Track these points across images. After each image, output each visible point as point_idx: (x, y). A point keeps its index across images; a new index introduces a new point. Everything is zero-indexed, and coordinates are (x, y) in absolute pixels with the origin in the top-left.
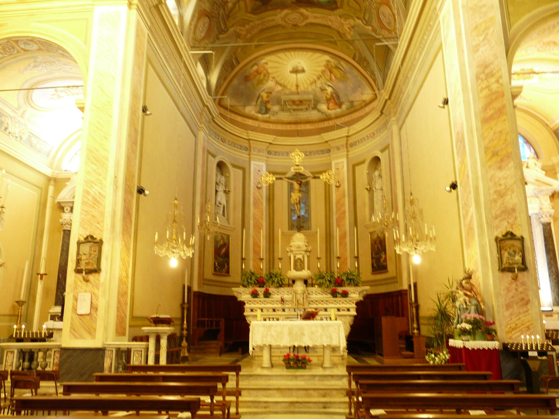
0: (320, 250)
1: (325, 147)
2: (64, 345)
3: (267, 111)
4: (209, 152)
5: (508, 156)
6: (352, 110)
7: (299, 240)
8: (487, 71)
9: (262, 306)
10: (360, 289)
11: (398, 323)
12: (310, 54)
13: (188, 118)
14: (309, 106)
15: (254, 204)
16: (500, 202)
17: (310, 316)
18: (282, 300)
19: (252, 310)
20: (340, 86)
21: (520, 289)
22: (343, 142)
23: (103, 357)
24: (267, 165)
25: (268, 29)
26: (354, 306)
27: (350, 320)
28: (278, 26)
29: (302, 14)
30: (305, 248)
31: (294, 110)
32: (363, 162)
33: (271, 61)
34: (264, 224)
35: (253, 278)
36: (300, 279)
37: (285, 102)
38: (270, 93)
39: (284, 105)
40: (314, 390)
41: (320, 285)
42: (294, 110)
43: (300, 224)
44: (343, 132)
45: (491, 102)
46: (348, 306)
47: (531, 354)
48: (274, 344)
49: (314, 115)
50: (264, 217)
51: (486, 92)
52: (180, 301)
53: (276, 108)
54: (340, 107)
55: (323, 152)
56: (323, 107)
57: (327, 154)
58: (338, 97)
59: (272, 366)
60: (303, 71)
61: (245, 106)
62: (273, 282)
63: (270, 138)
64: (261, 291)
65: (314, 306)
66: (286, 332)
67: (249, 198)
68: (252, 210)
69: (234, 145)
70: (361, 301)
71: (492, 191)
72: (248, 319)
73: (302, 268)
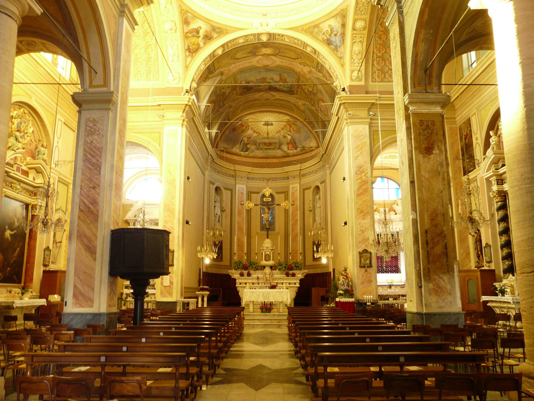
0: (280, 248)
1: (285, 175)
2: (158, 300)
3: (247, 150)
4: (211, 182)
5: (368, 213)
6: (304, 152)
7: (267, 243)
8: (361, 170)
9: (246, 281)
10: (302, 272)
11: (322, 292)
12: (277, 114)
13: (199, 163)
14: (275, 146)
15: (238, 214)
16: (362, 235)
17: (273, 287)
18: (258, 278)
19: (240, 284)
20: (296, 135)
21: (368, 276)
22: (297, 173)
23: (176, 306)
24: (246, 187)
25: (249, 101)
26: (299, 281)
27: (295, 290)
28: (256, 100)
29: (272, 95)
30: (271, 248)
31: (265, 149)
32: (309, 188)
33: (250, 118)
34: (245, 226)
35: (241, 265)
36: (268, 266)
37: (259, 143)
38: (250, 138)
39: (259, 146)
40: (274, 320)
41: (280, 269)
42: (265, 149)
43: (268, 228)
44: (298, 167)
45: (361, 186)
46: (295, 281)
47: (368, 304)
48: (255, 300)
49: (279, 153)
50: (245, 223)
51: (360, 180)
52: (197, 279)
53: (254, 147)
54: (296, 149)
55: (284, 179)
56: (285, 148)
57: (286, 180)
58: (295, 143)
59: (254, 312)
60: (272, 124)
61: (232, 148)
62: (253, 267)
63: (249, 169)
64: (245, 272)
65: (276, 281)
66: (261, 295)
67: (235, 211)
68: (237, 218)
69: (226, 174)
70: (302, 279)
71: (359, 230)
72: (238, 289)
73: (270, 260)
